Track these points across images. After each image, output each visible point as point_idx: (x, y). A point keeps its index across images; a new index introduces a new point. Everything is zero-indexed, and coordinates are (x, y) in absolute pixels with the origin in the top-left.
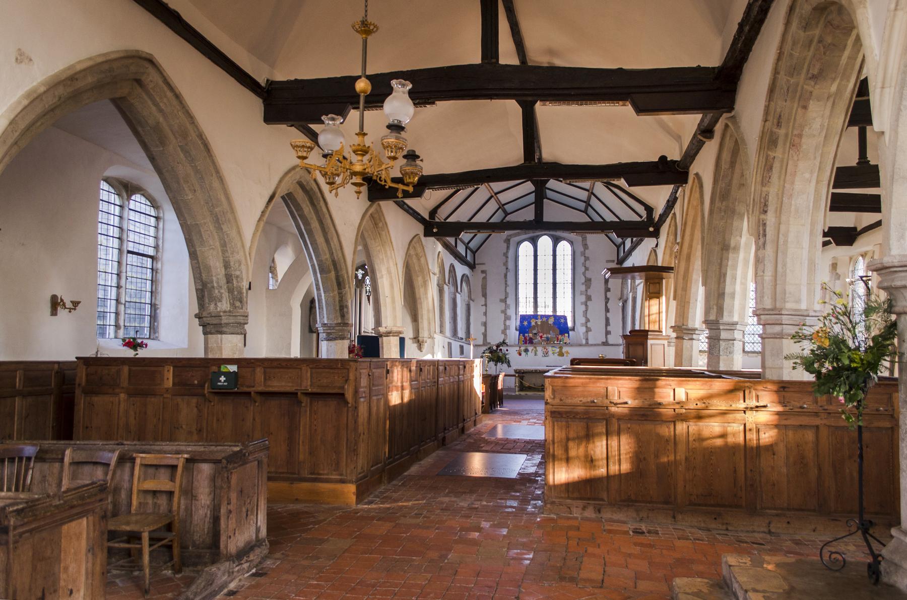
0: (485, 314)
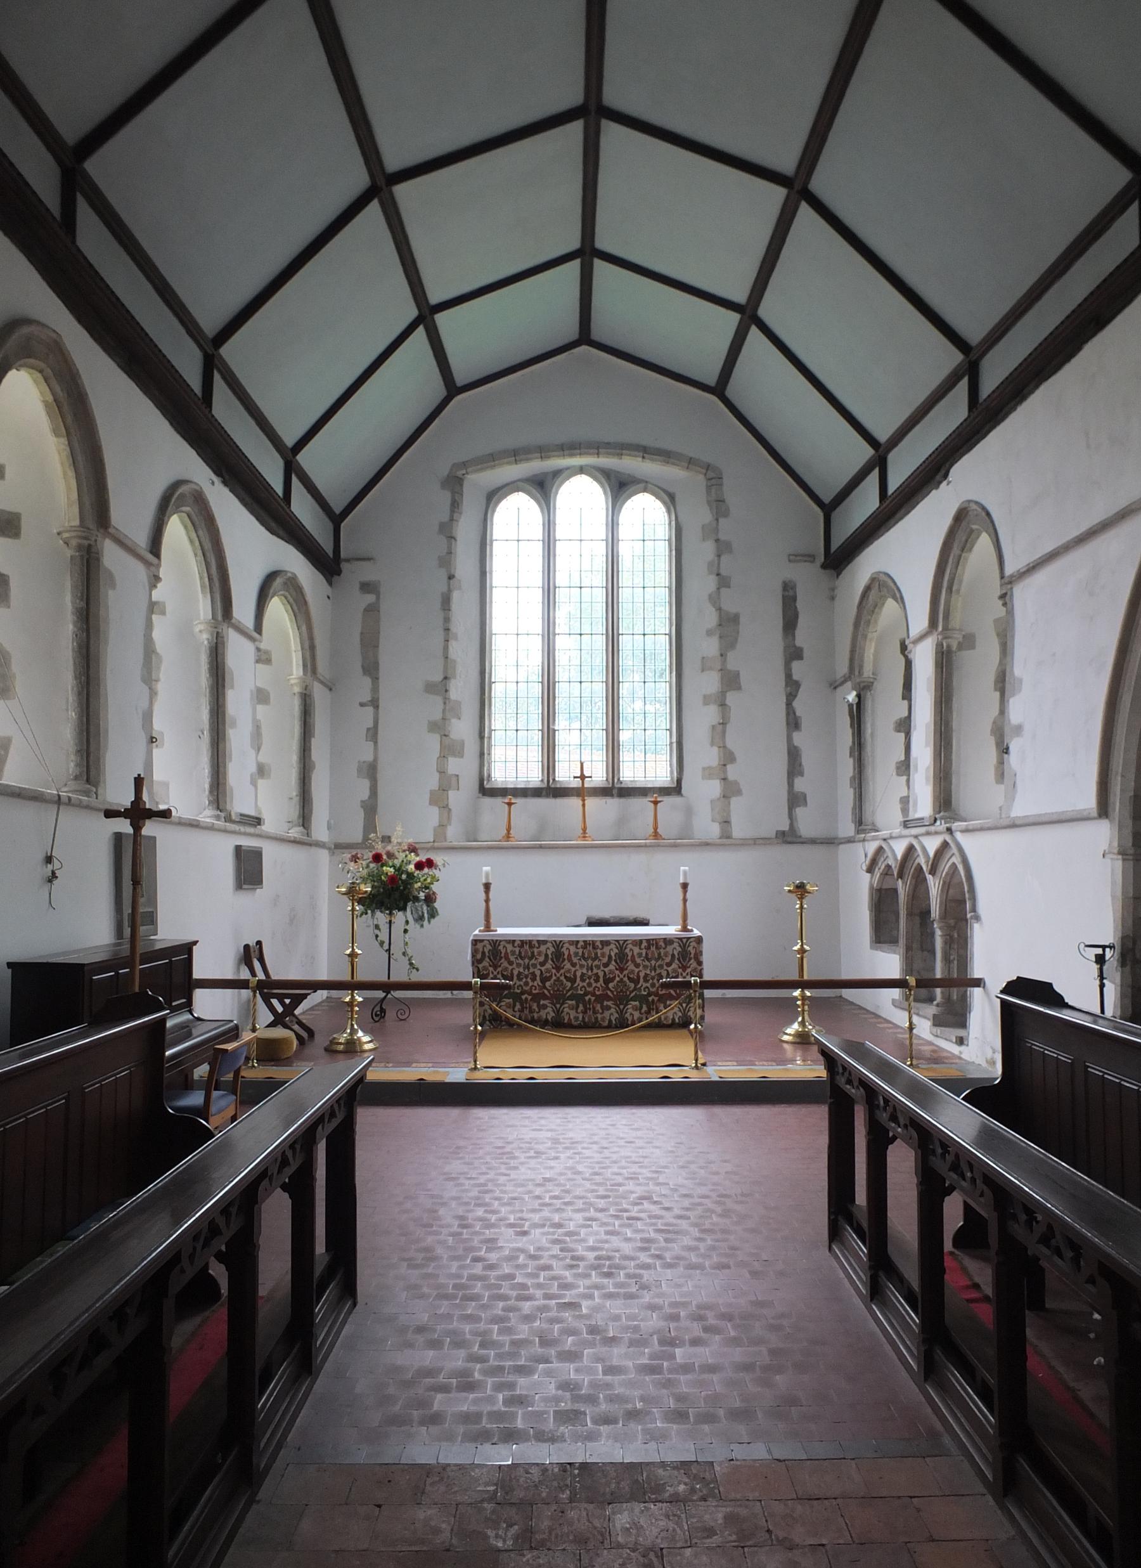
0: (373, 734)
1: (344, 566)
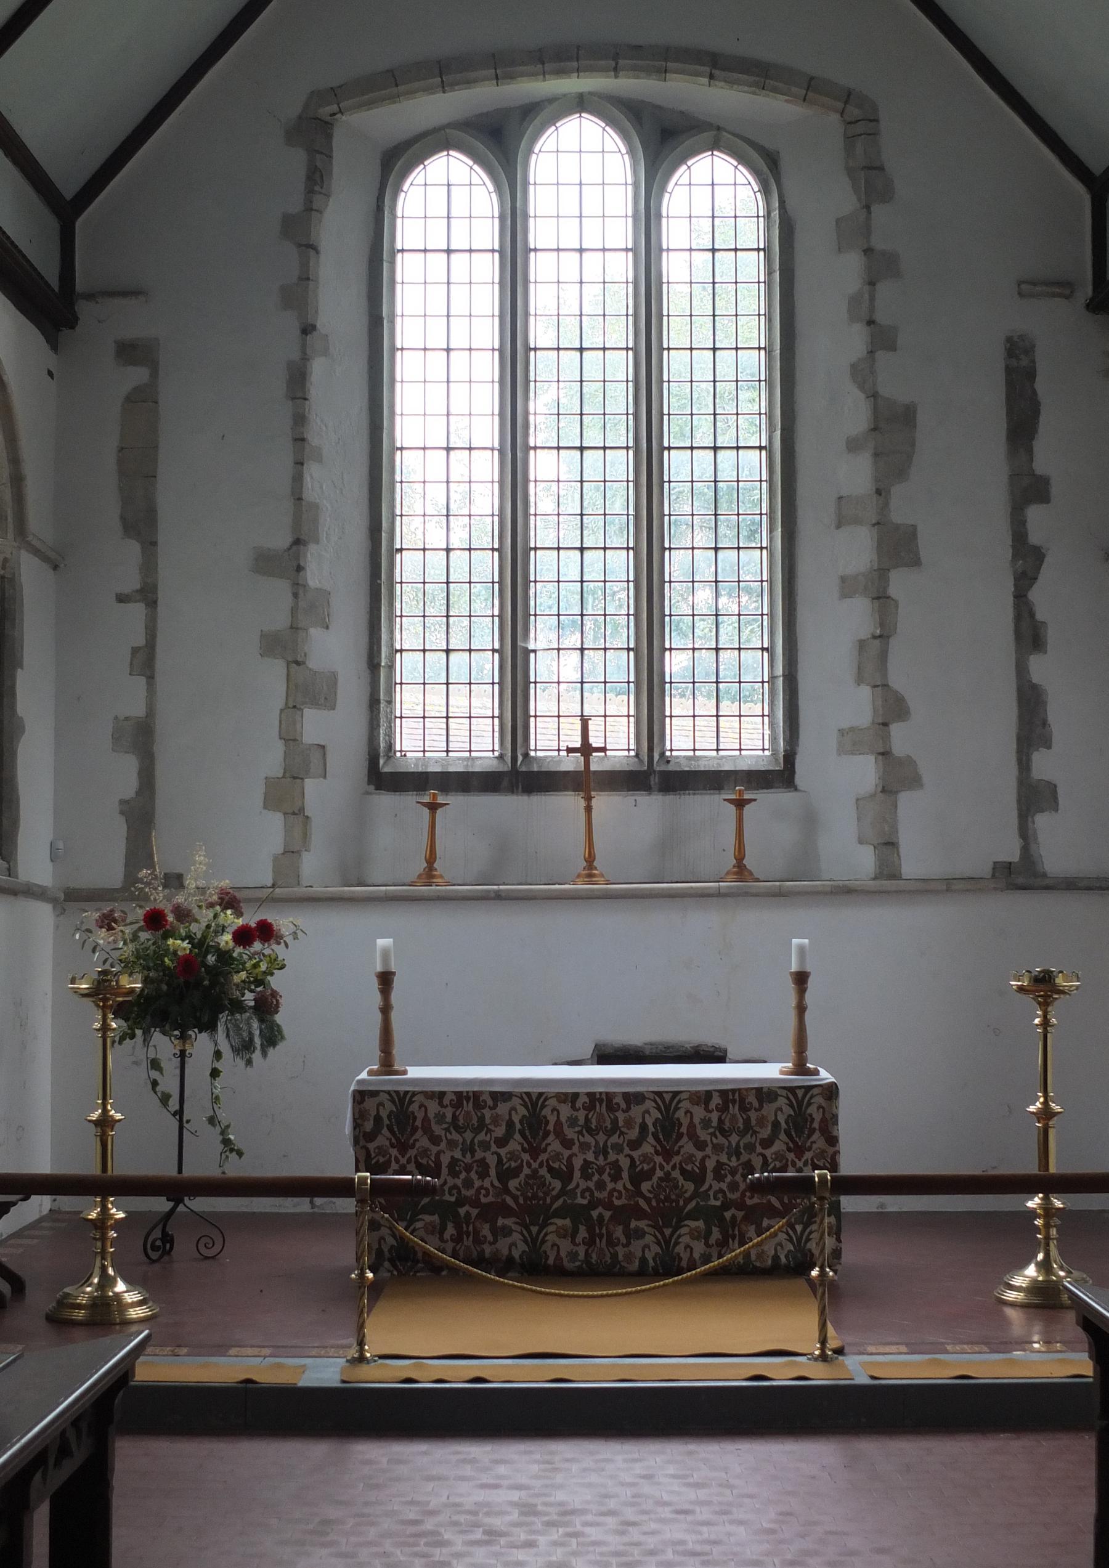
0: (145, 661)
1: (84, 309)
